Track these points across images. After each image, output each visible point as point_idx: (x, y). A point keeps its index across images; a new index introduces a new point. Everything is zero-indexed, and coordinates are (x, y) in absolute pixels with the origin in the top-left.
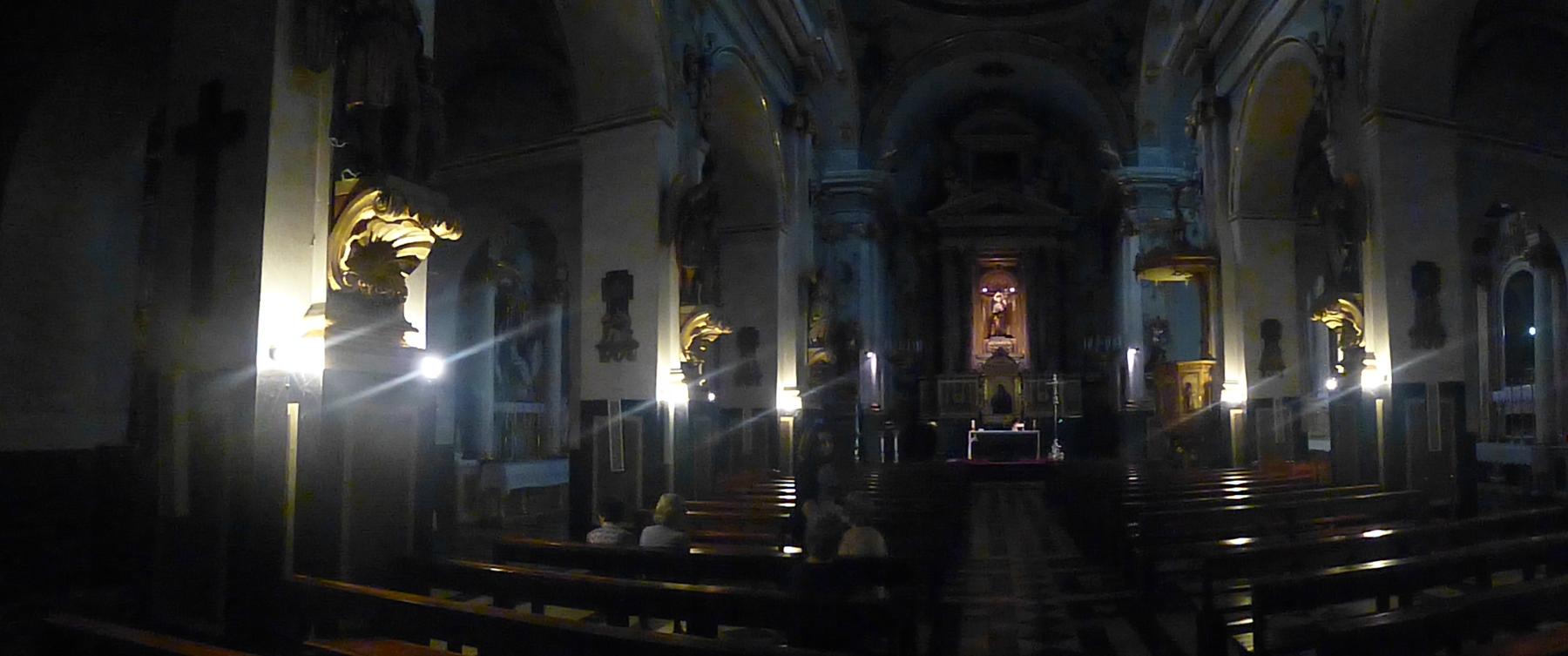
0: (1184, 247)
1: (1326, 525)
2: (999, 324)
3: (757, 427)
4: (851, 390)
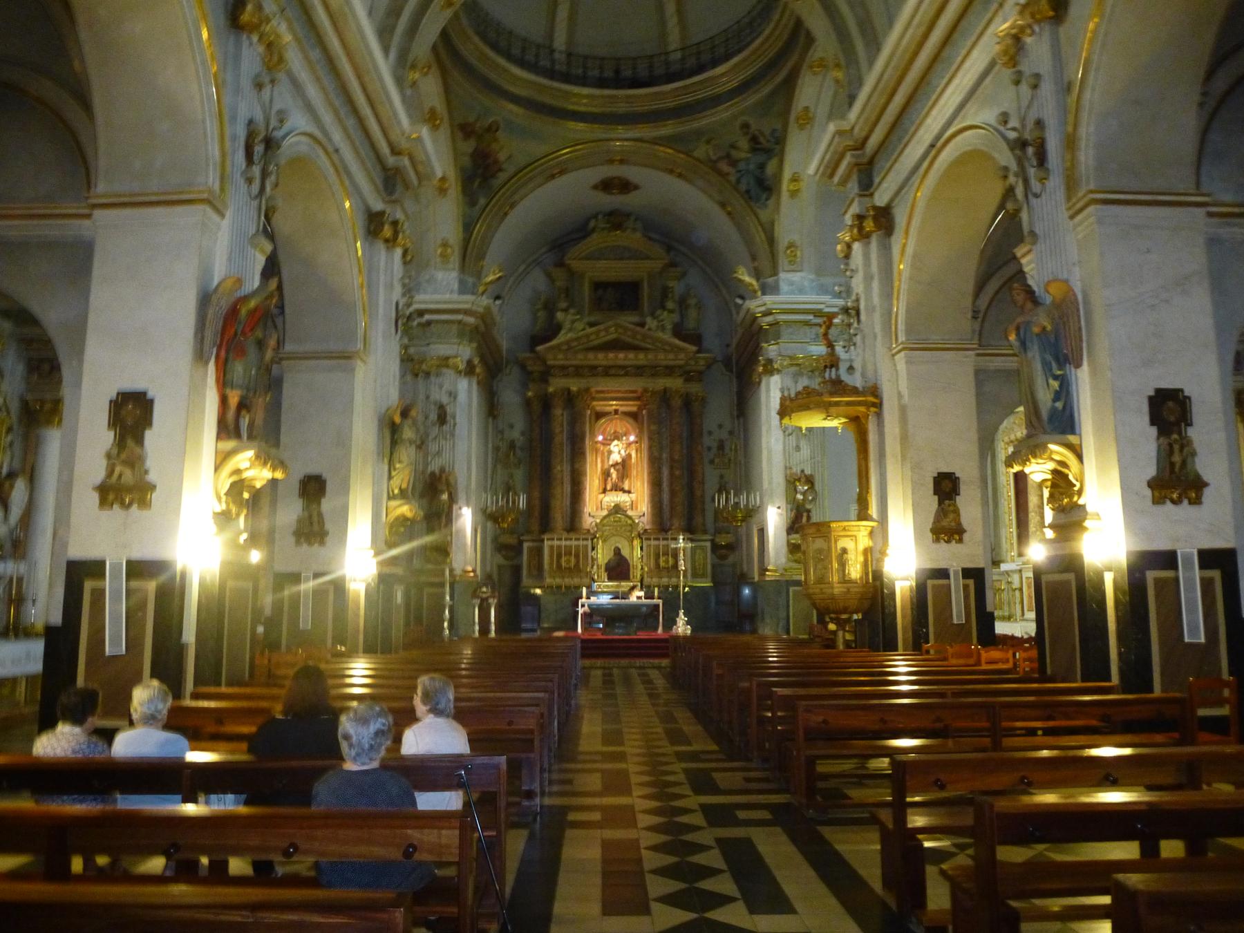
0: (838, 386)
1: (1032, 732)
2: (616, 479)
3: (319, 594)
4: (442, 551)
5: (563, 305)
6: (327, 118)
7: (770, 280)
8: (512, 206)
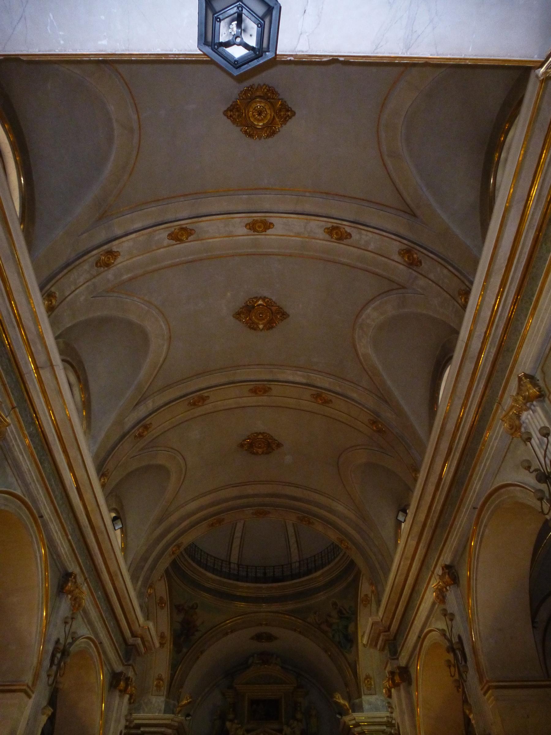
5: (231, 716)
6: (99, 625)
7: (357, 701)
8: (202, 653)
